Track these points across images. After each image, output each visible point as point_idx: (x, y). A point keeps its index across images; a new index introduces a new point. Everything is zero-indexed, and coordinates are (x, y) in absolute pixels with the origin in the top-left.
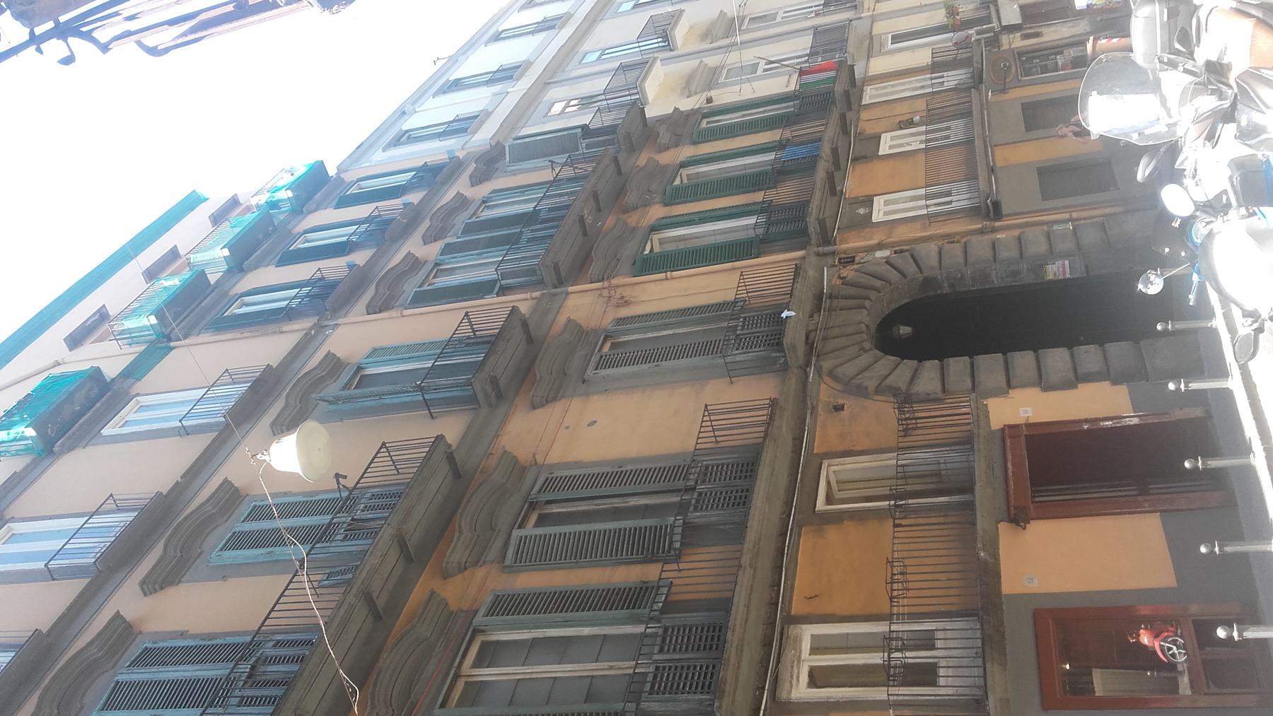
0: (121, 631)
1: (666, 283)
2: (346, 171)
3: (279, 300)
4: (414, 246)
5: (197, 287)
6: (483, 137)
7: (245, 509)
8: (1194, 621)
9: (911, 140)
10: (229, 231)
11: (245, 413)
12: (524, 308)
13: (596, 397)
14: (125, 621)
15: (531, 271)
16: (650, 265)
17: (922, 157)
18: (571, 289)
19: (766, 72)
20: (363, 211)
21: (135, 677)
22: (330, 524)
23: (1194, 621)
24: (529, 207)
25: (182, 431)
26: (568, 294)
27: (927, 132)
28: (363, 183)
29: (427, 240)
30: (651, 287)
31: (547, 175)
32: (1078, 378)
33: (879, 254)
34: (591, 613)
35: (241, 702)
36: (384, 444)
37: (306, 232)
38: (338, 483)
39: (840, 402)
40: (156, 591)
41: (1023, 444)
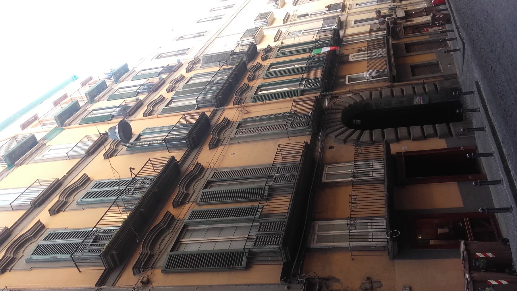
0: (40, 228)
1: (264, 106)
2: (136, 67)
3: (108, 112)
4: (162, 91)
5: (74, 108)
6: (190, 57)
7: (92, 184)
8: (411, 66)
9: (363, 56)
10: (87, 89)
11: (91, 152)
12: (208, 114)
13: (233, 145)
14: (42, 224)
15: (209, 101)
16: (257, 99)
17: (365, 63)
18: (225, 107)
19: (304, 31)
20: (142, 82)
21: (46, 243)
22: (125, 189)
23: (411, 66)
24: (209, 79)
25: (68, 158)
26: (224, 109)
27: (367, 54)
28: (120, 90)
29: (168, 91)
30: (258, 107)
31: (217, 69)
32: (425, 137)
33: (348, 95)
34: (231, 218)
35: (89, 251)
36: (150, 159)
37: (93, 110)
38: (131, 172)
39: (332, 145)
40: (55, 214)
41: (403, 159)
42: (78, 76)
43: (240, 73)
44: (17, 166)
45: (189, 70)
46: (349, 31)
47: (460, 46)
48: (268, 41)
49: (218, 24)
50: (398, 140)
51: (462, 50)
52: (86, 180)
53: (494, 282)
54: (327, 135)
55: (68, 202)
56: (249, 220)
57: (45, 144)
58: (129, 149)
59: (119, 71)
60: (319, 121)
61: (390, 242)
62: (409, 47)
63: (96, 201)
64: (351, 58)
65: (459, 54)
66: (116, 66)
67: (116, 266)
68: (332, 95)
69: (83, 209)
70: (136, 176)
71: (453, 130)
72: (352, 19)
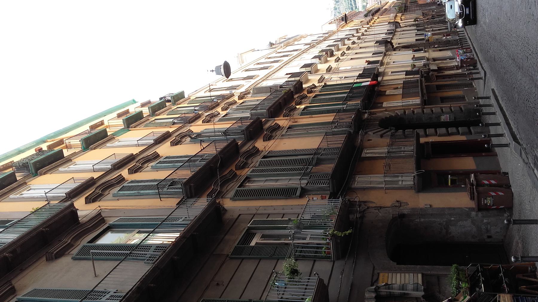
0: (122, 179)
42: (136, 100)
43: (287, 98)
44: (92, 149)
45: (240, 98)
46: (386, 78)
47: (482, 75)
48: (314, 79)
49: (266, 72)
50: (427, 136)
51: (483, 78)
52: (156, 156)
53: (494, 194)
54: (366, 133)
55: (142, 167)
56: (300, 174)
57: (114, 138)
58: (192, 140)
59: (177, 95)
60: (360, 124)
61: (416, 177)
62: (439, 87)
63: (168, 166)
64: (388, 92)
65: (482, 82)
66: (176, 91)
67: (191, 197)
68: (370, 112)
69: (157, 171)
70: (204, 148)
71: (472, 131)
72: (389, 71)
